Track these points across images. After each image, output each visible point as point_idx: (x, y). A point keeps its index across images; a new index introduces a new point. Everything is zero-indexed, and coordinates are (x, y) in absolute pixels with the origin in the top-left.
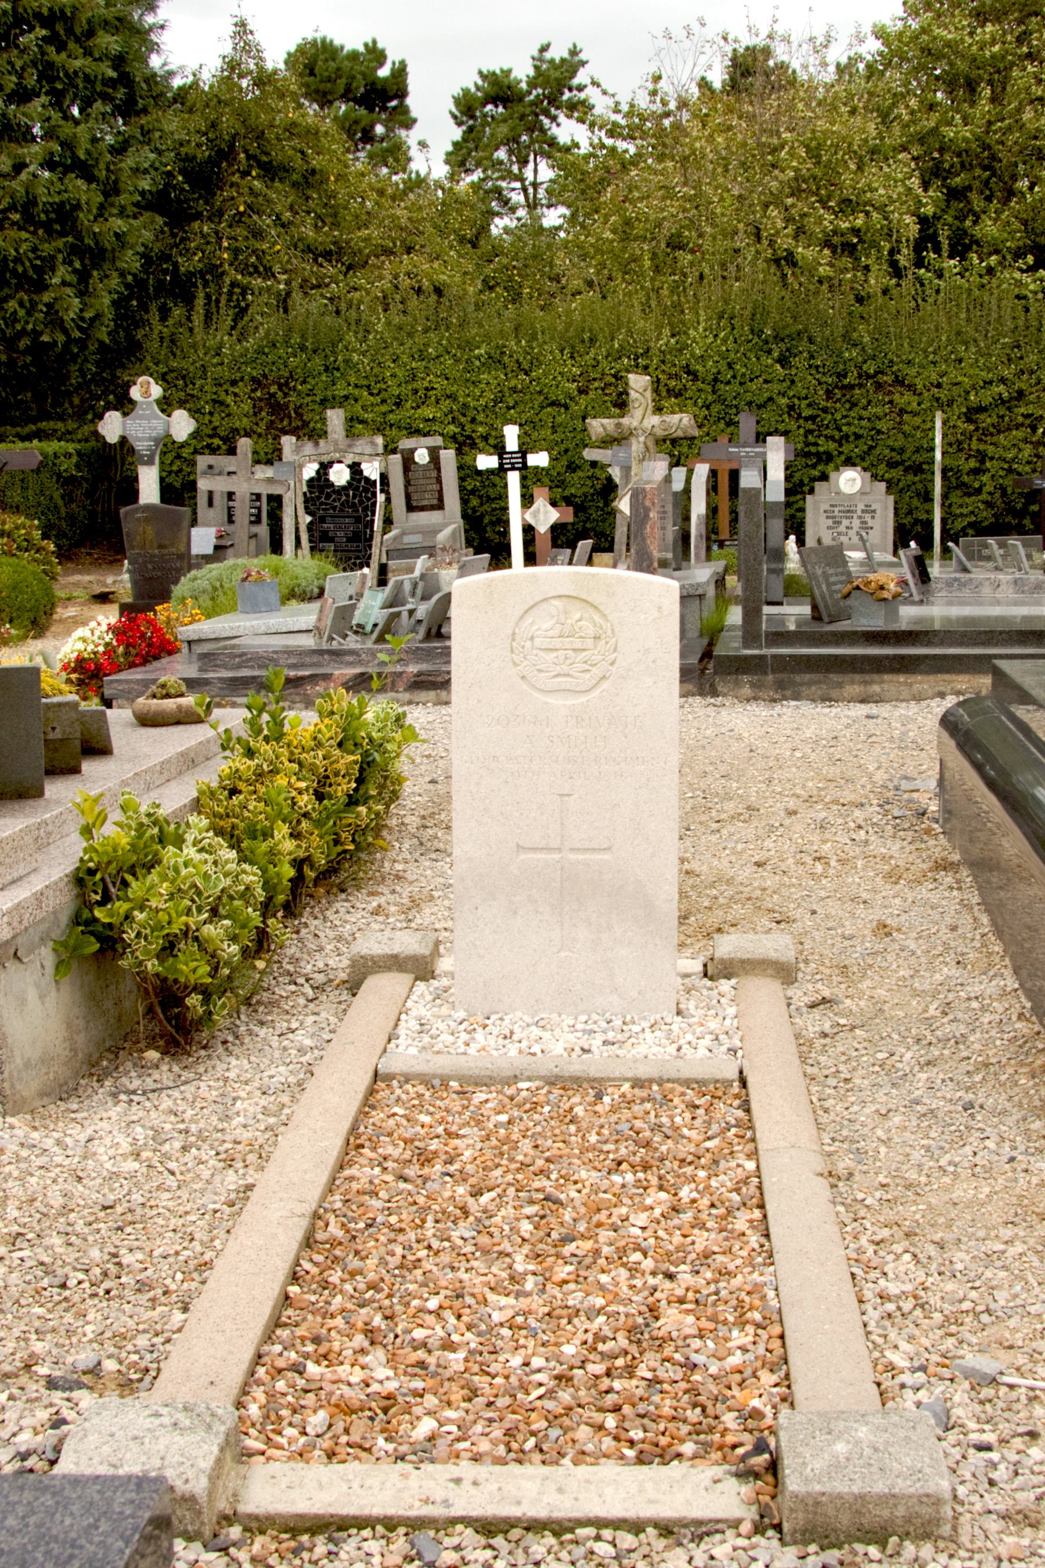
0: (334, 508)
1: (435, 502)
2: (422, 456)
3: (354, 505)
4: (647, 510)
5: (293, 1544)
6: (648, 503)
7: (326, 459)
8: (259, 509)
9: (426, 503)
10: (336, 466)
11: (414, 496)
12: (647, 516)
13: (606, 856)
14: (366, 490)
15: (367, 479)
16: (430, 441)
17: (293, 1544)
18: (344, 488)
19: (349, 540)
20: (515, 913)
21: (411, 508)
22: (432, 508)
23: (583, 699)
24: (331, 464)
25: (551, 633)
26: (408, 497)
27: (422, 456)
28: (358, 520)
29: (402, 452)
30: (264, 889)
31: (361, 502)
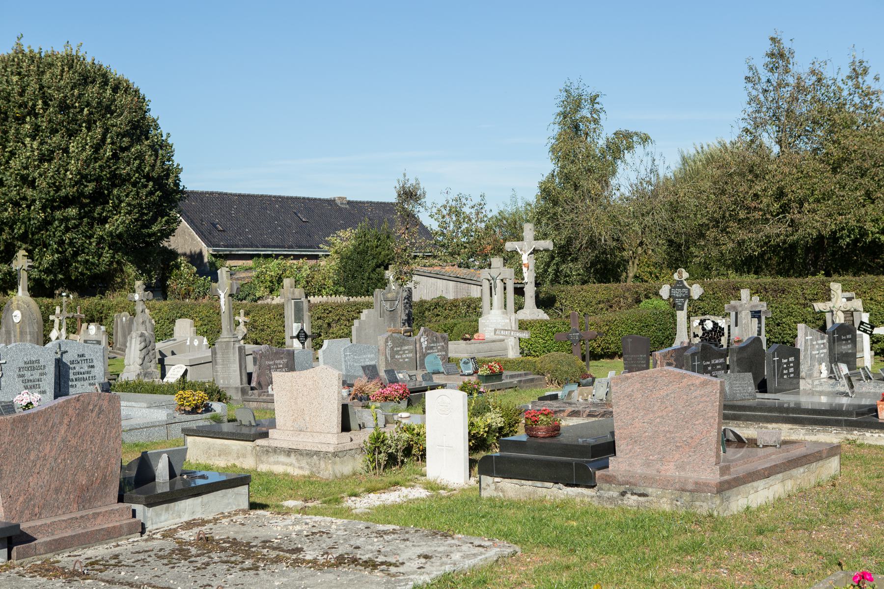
14: (720, 332)
15: (720, 328)
18: (711, 331)
24: (705, 320)
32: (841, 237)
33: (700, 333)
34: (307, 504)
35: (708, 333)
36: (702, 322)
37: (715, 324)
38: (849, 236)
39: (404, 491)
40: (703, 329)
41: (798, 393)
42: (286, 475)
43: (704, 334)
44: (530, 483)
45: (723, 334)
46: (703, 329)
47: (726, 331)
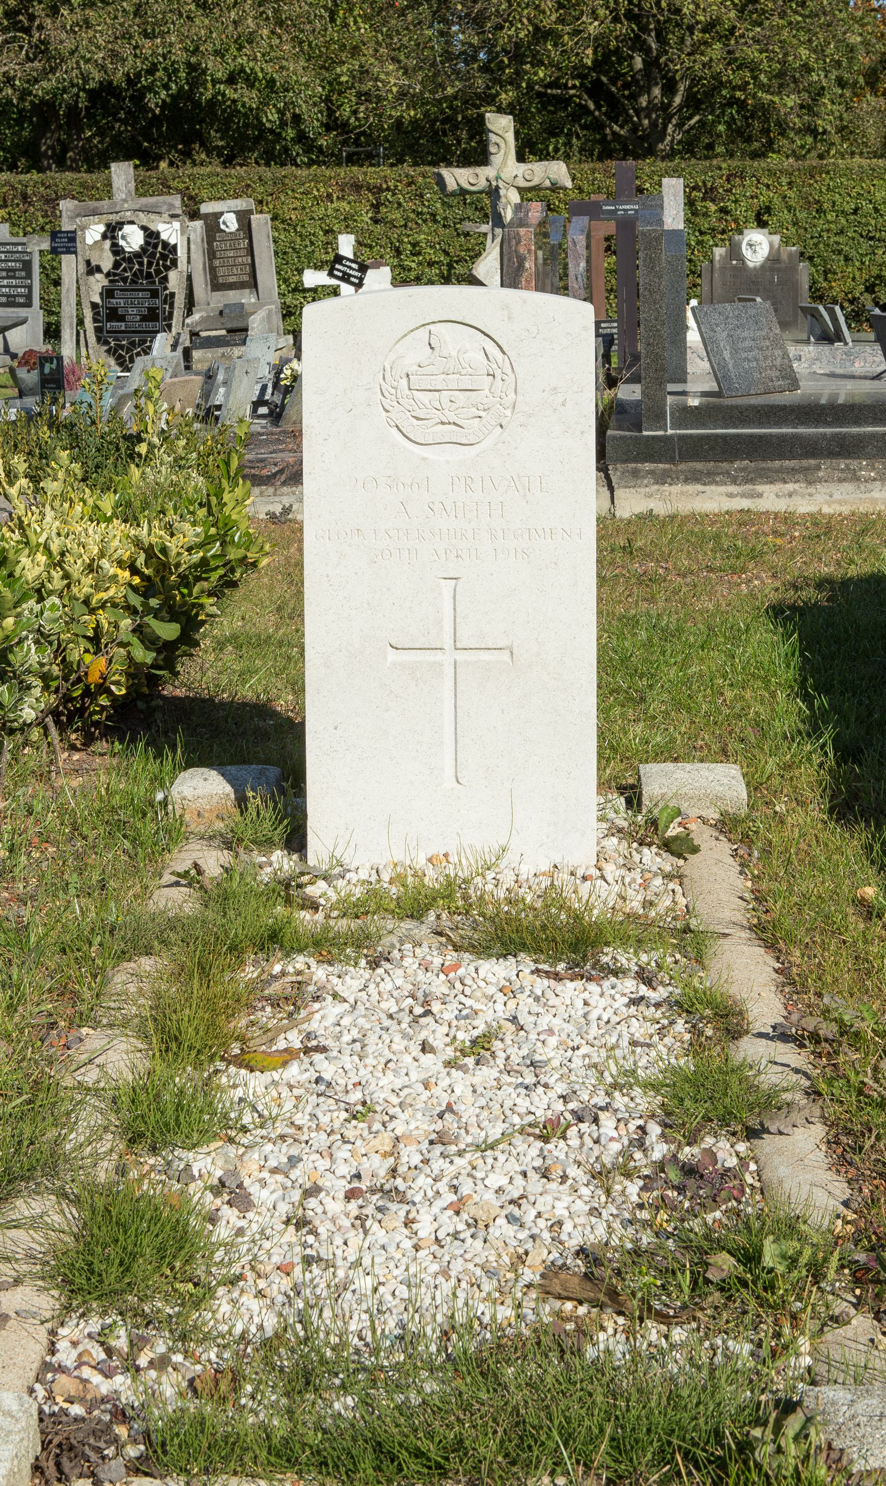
0: (125, 280)
1: (246, 278)
2: (230, 223)
3: (149, 276)
4: (521, 260)
5: (803, 1260)
6: (522, 250)
7: (114, 218)
8: (30, 288)
9: (232, 279)
10: (127, 229)
11: (221, 272)
12: (521, 265)
14: (164, 257)
15: (165, 244)
16: (241, 204)
17: (803, 1260)
18: (137, 255)
19: (144, 319)
21: (217, 286)
22: (241, 286)
24: (120, 225)
26: (213, 270)
27: (230, 223)
28: (154, 294)
29: (206, 217)
30: (124, 569)
31: (158, 272)
32: (150, 88)
33: (107, 262)
34: (354, 924)
35: (130, 260)
36: (112, 231)
37: (151, 236)
38: (166, 87)
39: (661, 508)
40: (116, 250)
41: (685, 381)
42: (764, 459)
43: (116, 265)
44: (778, 487)
45: (174, 263)
46: (116, 250)
47: (181, 253)
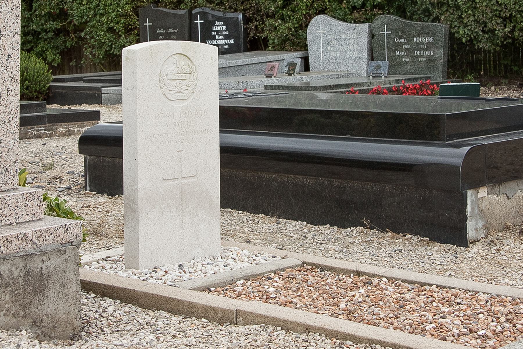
13: (195, 179)
20: (163, 213)
23: (185, 103)
25: (174, 72)
